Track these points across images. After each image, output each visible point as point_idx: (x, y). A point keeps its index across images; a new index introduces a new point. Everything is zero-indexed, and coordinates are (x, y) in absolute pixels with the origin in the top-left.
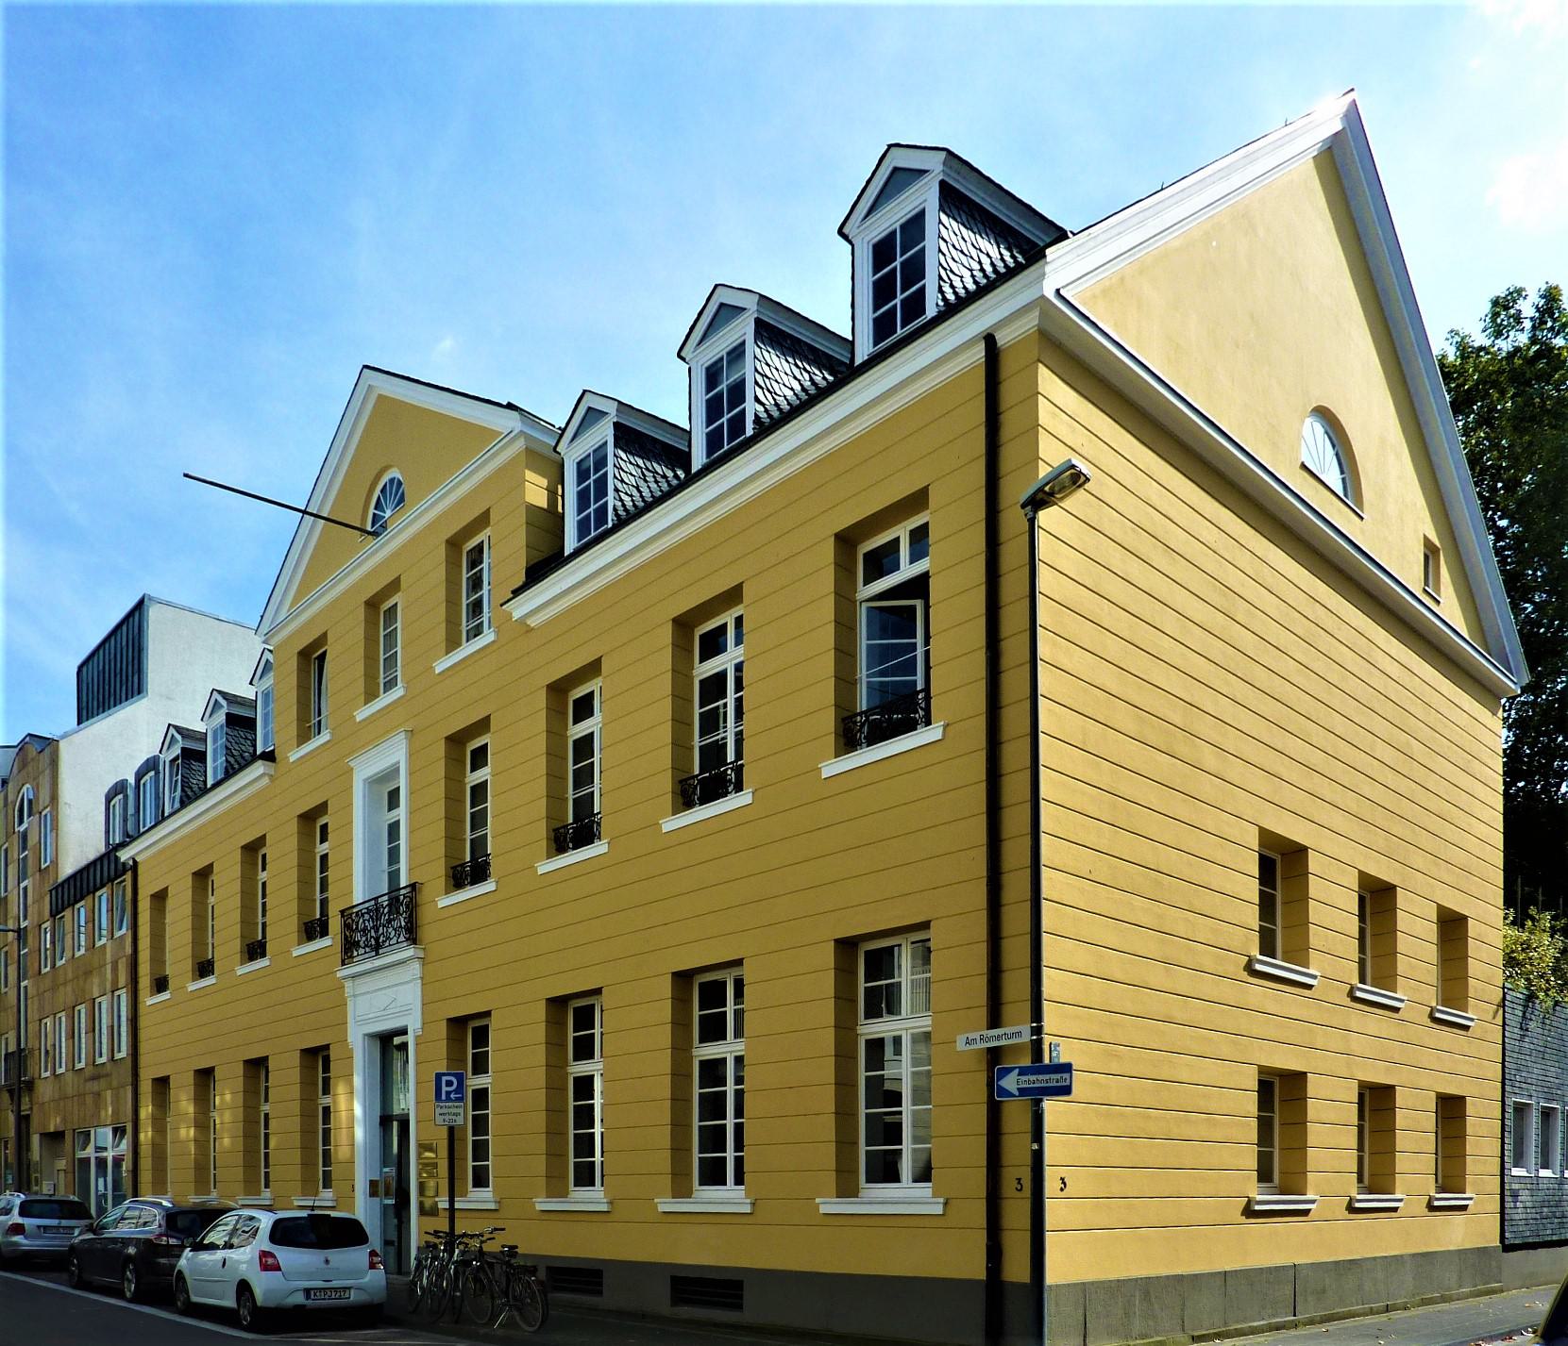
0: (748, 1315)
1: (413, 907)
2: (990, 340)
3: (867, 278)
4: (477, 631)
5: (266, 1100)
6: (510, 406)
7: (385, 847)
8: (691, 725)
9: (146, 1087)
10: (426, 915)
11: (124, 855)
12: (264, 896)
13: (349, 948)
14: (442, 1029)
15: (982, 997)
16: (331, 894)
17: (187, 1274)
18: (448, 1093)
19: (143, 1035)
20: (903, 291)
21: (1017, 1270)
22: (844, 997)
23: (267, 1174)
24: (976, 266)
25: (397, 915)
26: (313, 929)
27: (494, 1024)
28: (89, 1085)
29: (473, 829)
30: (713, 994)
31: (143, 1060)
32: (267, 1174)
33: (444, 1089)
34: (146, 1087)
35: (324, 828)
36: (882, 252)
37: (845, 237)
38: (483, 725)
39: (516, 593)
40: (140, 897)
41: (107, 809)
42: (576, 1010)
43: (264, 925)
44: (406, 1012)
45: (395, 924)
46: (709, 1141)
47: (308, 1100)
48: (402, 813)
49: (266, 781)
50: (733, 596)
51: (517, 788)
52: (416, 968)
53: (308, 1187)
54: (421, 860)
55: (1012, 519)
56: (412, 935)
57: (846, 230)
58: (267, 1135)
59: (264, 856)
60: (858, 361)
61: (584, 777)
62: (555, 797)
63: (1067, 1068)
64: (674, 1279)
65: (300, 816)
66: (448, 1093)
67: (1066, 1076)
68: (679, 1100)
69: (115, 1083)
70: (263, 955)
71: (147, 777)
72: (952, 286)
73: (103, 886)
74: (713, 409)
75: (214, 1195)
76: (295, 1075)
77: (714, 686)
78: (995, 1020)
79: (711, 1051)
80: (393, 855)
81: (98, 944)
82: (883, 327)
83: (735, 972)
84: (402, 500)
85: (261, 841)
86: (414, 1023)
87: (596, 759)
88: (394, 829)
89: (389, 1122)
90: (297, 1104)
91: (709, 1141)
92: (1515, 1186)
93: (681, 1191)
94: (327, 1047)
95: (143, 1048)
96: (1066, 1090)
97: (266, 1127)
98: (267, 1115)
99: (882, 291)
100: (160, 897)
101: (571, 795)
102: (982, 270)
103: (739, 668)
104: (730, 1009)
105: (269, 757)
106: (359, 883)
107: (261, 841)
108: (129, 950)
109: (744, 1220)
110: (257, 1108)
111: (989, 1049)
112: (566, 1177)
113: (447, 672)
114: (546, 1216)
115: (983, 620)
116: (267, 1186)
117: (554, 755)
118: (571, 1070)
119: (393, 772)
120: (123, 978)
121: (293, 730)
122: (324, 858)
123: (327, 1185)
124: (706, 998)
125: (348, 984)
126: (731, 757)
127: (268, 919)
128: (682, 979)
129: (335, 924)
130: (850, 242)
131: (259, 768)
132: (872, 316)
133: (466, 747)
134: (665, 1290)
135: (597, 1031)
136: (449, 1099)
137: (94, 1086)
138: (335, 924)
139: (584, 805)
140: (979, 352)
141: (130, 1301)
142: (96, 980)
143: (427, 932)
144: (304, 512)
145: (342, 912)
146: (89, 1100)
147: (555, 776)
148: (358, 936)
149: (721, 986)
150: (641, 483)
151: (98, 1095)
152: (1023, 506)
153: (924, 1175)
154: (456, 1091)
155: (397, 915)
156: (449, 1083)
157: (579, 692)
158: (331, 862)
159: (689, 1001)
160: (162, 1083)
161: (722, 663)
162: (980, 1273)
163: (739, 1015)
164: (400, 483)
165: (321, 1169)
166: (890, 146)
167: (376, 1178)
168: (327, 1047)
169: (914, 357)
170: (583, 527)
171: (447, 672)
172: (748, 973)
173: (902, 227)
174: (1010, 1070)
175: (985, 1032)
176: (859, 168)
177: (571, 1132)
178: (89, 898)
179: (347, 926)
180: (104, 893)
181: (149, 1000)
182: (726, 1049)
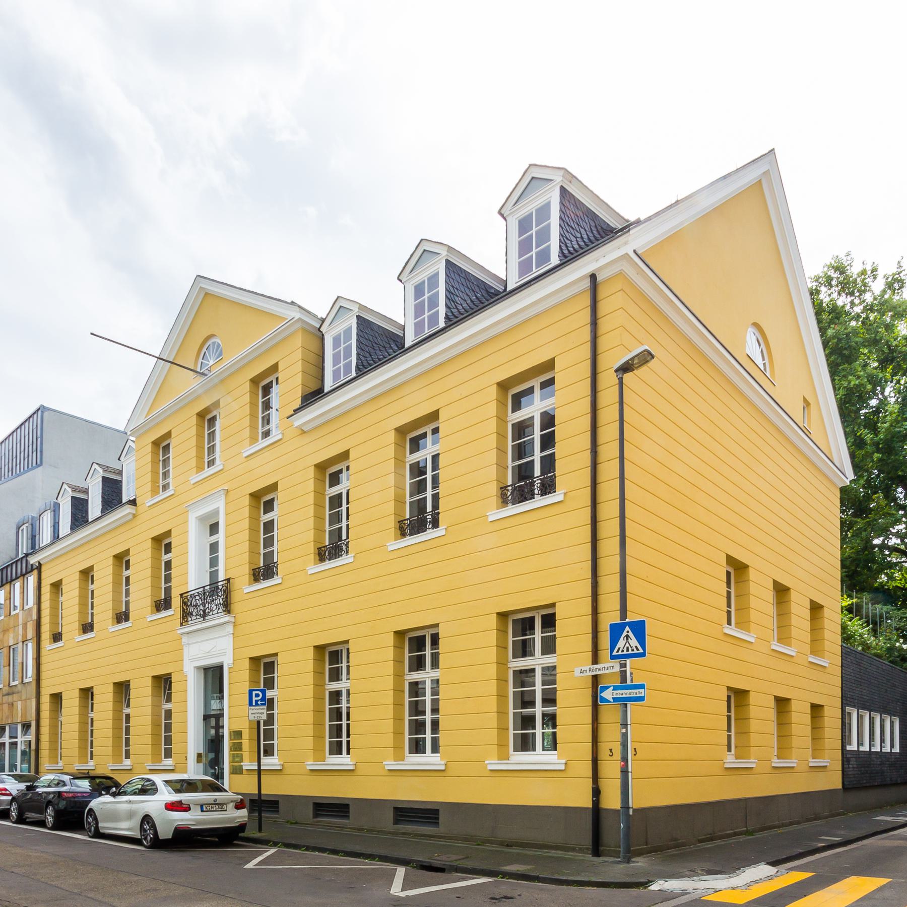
0: (442, 829)
1: (227, 592)
2: (593, 277)
3: (515, 239)
4: (267, 434)
5: (92, 711)
6: (293, 303)
7: (208, 557)
8: (259, 543)
9: (45, 700)
10: (236, 597)
11: (33, 560)
12: (92, 598)
13: (186, 616)
14: (246, 664)
15: (589, 646)
16: (173, 583)
17: (95, 809)
18: (257, 701)
19: (43, 668)
20: (429, 311)
21: (611, 800)
22: (318, 673)
23: (92, 752)
24: (579, 235)
25: (219, 594)
26: (163, 604)
27: (442, 632)
28: (5, 698)
29: (165, 583)
30: (335, 657)
31: (44, 683)
32: (92, 752)
33: (254, 699)
34: (45, 700)
35: (128, 562)
36: (524, 225)
37: (502, 215)
38: (274, 487)
39: (296, 411)
40: (43, 585)
41: (18, 533)
42: (330, 652)
43: (92, 614)
44: (224, 654)
45: (217, 602)
46: (420, 726)
47: (117, 711)
48: (221, 537)
49: (131, 517)
50: (345, 455)
51: (297, 525)
52: (230, 629)
53: (116, 757)
54: (235, 564)
55: (608, 379)
56: (227, 607)
57: (502, 212)
58: (92, 731)
59: (92, 576)
60: (407, 346)
61: (269, 542)
62: (253, 552)
63: (641, 686)
64: (396, 809)
65: (80, 572)
66: (257, 701)
67: (642, 690)
68: (318, 711)
69: (24, 698)
70: (92, 630)
71: (24, 527)
72: (567, 246)
73: (17, 578)
74: (419, 310)
75: (60, 764)
76: (77, 701)
77: (336, 501)
78: (595, 661)
79: (416, 676)
80: (214, 562)
81: (13, 613)
82: (525, 267)
83: (346, 646)
84: (221, 354)
85: (91, 568)
86: (227, 661)
87: (275, 533)
88: (214, 547)
89: (213, 720)
90: (111, 713)
91: (420, 726)
92: (848, 756)
93: (400, 758)
94: (92, 688)
95: (44, 675)
96: (641, 699)
97: (92, 726)
98: (92, 719)
99: (525, 247)
100: (57, 586)
101: (163, 586)
102: (582, 238)
103: (435, 458)
104: (344, 665)
105: (133, 502)
106: (191, 576)
107: (91, 568)
108: (35, 617)
109: (560, 774)
110: (87, 715)
111: (593, 676)
112: (324, 750)
113: (243, 460)
114: (494, 774)
115: (589, 433)
116: (92, 758)
117: (253, 530)
118: (406, 677)
119: (216, 512)
120: (31, 633)
121: (149, 487)
122: (128, 579)
123: (128, 756)
124: (332, 658)
125: (185, 640)
126: (429, 508)
127: (95, 611)
128: (320, 649)
129: (176, 602)
130: (505, 219)
131: (127, 510)
132: (518, 260)
133: (264, 500)
134: (390, 815)
135: (275, 675)
136: (257, 704)
137: (9, 699)
138: (176, 602)
139: (269, 556)
140: (587, 283)
141: (49, 829)
142: (11, 635)
143: (236, 607)
144: (159, 358)
145: (181, 595)
146: (6, 707)
147: (253, 541)
148: (192, 609)
149: (532, 619)
150: (372, 350)
151: (11, 705)
152: (616, 371)
153: (435, 749)
154: (261, 700)
155: (219, 594)
156: (257, 695)
157: (268, 497)
158: (442, 461)
159: (506, 632)
160: (57, 698)
161: (424, 455)
162: (586, 802)
163: (348, 667)
164: (219, 345)
165: (124, 748)
166: (530, 165)
167: (201, 751)
168: (92, 688)
169: (451, 337)
170: (336, 374)
171: (243, 460)
172: (351, 646)
173: (429, 279)
174: (607, 688)
175: (592, 667)
176: (508, 180)
177: (163, 734)
178: (7, 587)
179: (184, 603)
180: (18, 585)
181: (47, 645)
182: (426, 676)
